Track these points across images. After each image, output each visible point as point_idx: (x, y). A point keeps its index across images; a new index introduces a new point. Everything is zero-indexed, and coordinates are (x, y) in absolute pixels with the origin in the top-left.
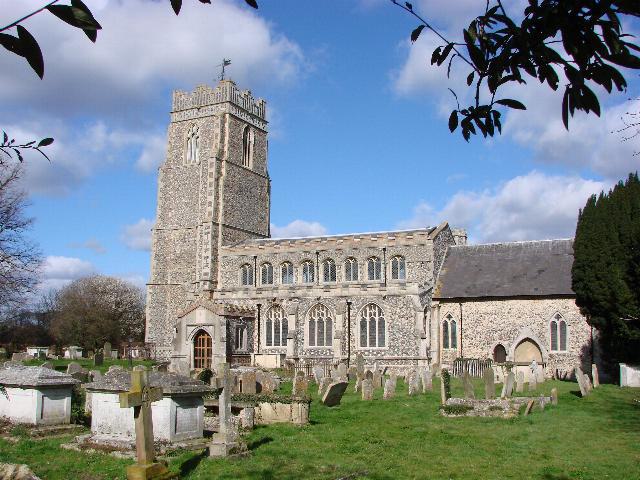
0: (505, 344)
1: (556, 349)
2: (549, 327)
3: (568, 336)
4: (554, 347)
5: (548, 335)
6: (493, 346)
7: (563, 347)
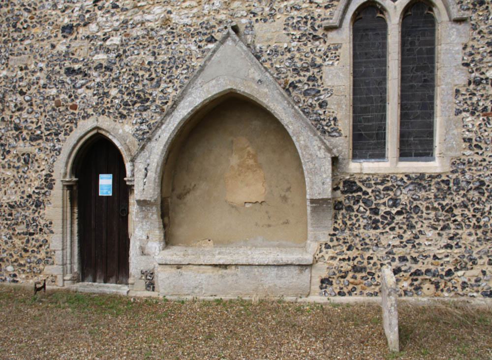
0: (122, 133)
1: (380, 155)
2: (344, 37)
3: (449, 75)
4: (368, 141)
5: (338, 77)
6: (69, 143)
7: (416, 143)
